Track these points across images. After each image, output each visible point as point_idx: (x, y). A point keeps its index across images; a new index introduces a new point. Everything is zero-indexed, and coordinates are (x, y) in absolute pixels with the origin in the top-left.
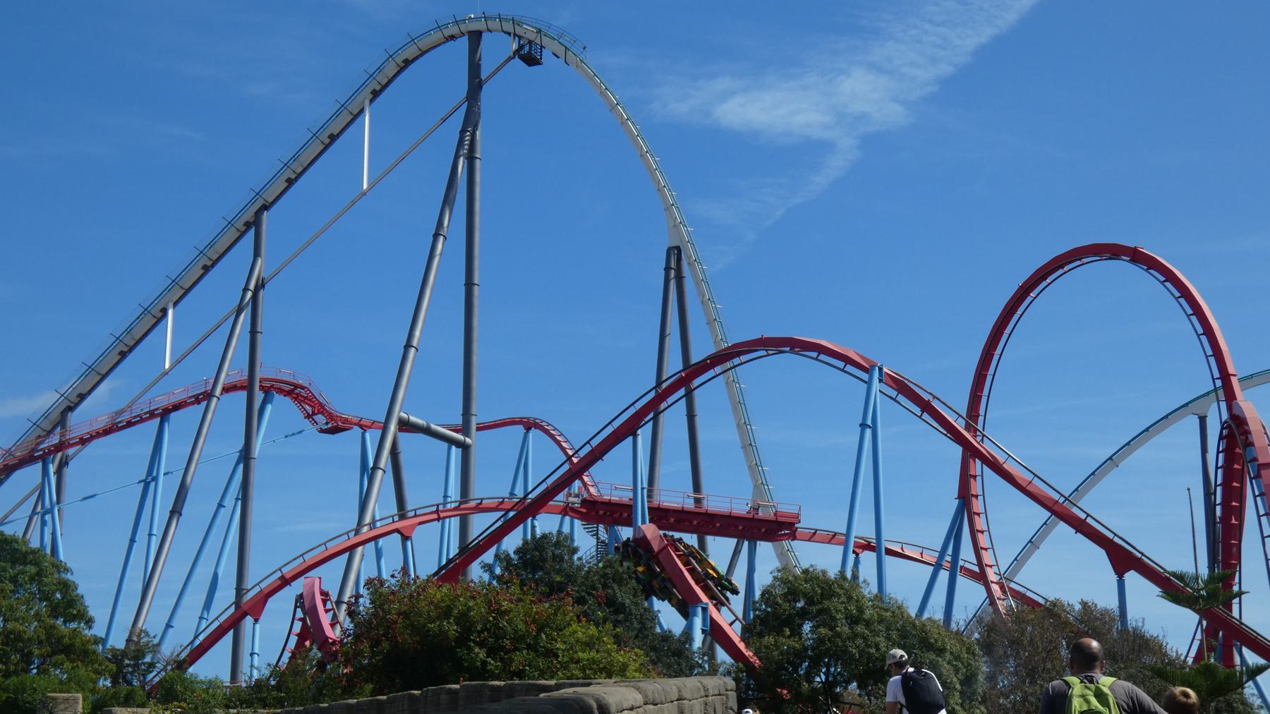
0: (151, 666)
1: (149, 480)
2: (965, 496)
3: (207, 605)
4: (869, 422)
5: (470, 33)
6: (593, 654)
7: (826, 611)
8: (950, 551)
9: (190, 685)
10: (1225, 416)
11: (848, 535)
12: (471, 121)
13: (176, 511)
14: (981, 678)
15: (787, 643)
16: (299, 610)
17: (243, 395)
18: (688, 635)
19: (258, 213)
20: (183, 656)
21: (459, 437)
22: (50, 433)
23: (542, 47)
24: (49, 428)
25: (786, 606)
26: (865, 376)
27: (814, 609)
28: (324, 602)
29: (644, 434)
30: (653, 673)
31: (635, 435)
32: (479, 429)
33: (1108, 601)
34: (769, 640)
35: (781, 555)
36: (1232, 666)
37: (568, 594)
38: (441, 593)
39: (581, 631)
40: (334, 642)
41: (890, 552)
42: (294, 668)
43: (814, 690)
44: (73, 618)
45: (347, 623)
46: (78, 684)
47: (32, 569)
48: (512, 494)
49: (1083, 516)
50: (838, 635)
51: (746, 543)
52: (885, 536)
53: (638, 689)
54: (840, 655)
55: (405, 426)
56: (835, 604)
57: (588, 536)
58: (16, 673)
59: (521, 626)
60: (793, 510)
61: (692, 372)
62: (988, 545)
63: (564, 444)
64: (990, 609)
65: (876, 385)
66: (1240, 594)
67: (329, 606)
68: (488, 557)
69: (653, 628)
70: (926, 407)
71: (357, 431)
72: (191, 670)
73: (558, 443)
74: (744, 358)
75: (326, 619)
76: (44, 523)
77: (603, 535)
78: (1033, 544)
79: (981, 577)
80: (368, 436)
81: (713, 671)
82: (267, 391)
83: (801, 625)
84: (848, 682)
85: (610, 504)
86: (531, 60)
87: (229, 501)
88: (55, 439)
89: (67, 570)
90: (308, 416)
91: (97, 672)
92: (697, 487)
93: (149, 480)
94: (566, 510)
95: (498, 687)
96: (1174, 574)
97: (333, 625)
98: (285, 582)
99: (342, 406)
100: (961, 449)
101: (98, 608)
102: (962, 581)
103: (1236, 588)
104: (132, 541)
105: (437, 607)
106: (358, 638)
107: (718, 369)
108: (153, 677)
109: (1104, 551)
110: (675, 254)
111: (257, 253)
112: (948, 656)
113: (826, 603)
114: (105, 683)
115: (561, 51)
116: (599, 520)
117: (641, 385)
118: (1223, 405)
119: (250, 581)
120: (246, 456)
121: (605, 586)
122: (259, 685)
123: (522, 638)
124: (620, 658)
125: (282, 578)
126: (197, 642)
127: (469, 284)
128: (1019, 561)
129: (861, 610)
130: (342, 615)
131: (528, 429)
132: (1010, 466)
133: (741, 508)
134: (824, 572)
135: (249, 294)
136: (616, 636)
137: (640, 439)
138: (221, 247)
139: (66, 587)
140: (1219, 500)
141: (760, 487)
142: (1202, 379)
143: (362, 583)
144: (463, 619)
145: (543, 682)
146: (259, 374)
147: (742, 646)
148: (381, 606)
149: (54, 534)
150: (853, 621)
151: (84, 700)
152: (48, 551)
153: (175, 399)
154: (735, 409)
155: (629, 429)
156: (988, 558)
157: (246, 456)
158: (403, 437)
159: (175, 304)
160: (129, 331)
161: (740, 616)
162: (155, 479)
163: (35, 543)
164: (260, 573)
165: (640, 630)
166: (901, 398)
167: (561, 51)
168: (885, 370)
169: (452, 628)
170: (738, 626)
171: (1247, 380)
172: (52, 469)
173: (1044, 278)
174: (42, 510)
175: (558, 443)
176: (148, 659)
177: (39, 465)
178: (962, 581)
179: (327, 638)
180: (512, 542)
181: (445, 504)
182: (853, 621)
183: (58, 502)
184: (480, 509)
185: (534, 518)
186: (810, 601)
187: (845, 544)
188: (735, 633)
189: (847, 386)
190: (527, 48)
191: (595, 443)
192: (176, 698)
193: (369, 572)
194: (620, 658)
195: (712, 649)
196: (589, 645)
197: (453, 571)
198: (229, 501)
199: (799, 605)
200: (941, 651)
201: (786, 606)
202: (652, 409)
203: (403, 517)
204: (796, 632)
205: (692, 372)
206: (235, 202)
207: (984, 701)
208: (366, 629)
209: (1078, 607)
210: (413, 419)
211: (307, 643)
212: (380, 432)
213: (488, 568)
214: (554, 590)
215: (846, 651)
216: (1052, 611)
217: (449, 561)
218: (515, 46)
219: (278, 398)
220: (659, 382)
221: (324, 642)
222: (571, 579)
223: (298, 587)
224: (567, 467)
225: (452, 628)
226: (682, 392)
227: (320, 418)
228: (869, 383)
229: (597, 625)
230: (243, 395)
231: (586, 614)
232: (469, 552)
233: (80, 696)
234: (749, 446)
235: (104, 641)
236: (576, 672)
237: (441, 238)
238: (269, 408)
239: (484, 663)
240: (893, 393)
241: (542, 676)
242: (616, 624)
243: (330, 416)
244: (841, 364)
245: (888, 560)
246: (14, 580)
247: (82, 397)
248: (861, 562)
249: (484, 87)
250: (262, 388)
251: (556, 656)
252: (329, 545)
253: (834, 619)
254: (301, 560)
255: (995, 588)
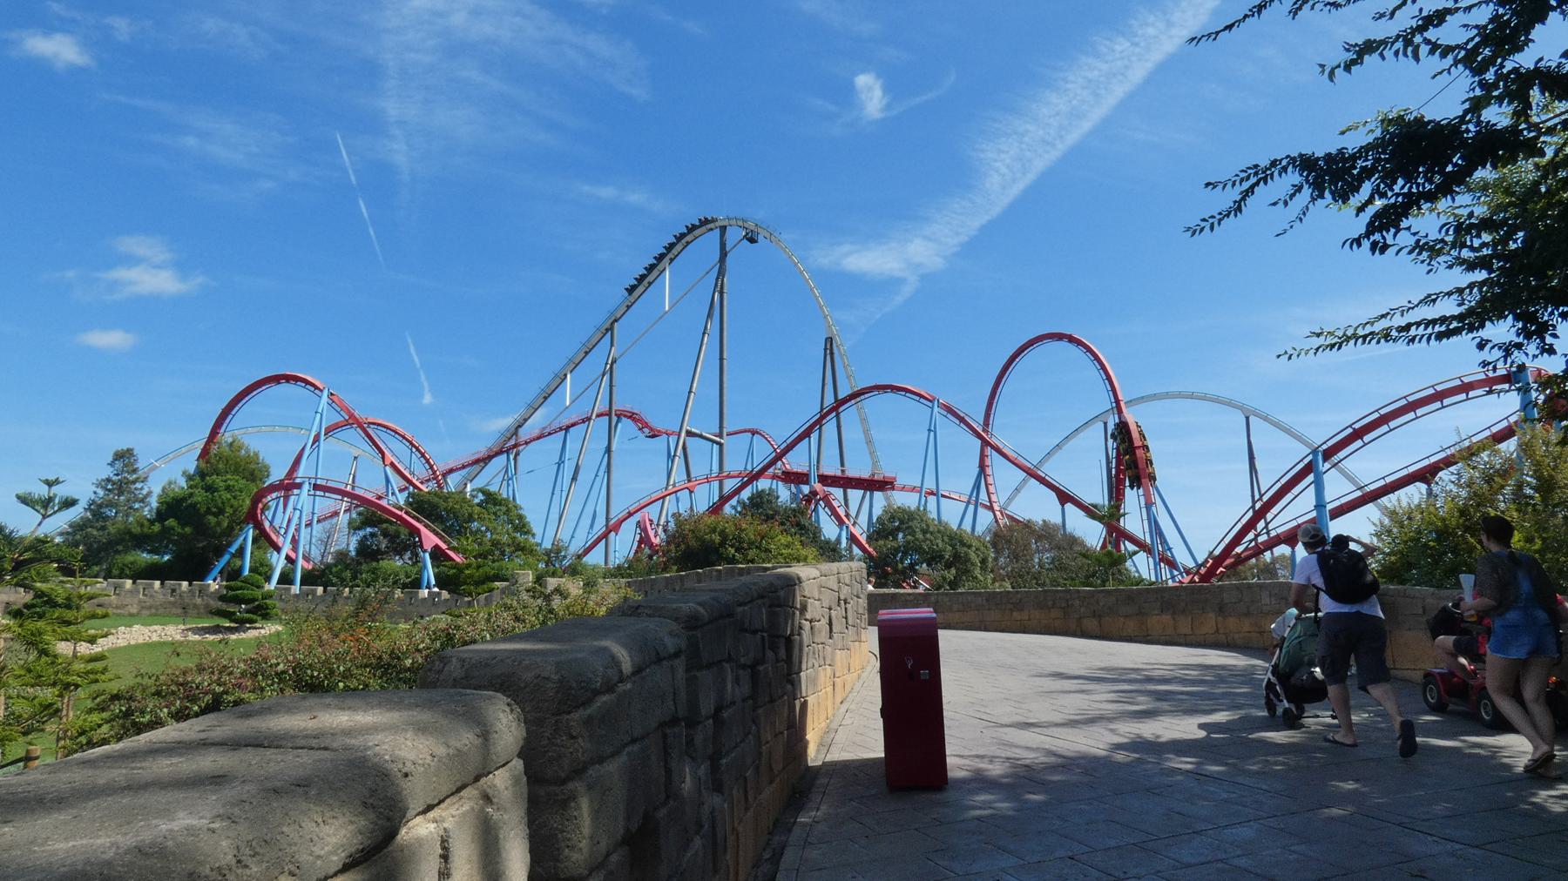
0: (565, 557)
1: (560, 463)
2: (982, 467)
3: (592, 526)
4: (932, 429)
5: (720, 227)
6: (790, 550)
7: (910, 527)
8: (975, 494)
9: (585, 566)
10: (1117, 421)
11: (921, 488)
12: (721, 273)
13: (574, 479)
14: (990, 560)
15: (890, 544)
16: (638, 529)
17: (607, 418)
18: (838, 540)
19: (612, 324)
20: (580, 552)
21: (718, 439)
22: (510, 439)
23: (758, 233)
24: (509, 436)
25: (890, 525)
26: (930, 404)
27: (904, 526)
28: (651, 525)
29: (814, 436)
30: (821, 560)
31: (810, 437)
32: (727, 435)
33: (1056, 519)
34: (881, 542)
35: (887, 499)
36: (1120, 551)
37: (776, 521)
38: (711, 520)
39: (784, 539)
40: (656, 545)
41: (943, 496)
42: (637, 559)
43: (904, 567)
44: (526, 533)
45: (663, 535)
46: (529, 565)
47: (504, 509)
48: (746, 469)
49: (1044, 476)
50: (917, 539)
51: (868, 493)
52: (941, 487)
53: (817, 569)
54: (918, 550)
55: (689, 434)
56: (915, 524)
57: (786, 490)
58: (498, 561)
59: (752, 537)
60: (894, 475)
61: (839, 403)
62: (994, 491)
63: (772, 443)
64: (995, 525)
65: (936, 409)
66: (1124, 515)
67: (653, 527)
68: (734, 501)
69: (820, 536)
70: (962, 420)
71: (665, 436)
72: (584, 559)
73: (766, 439)
74: (866, 396)
75: (652, 534)
76: (508, 485)
77: (794, 490)
78: (1017, 490)
79: (991, 508)
80: (670, 438)
81: (852, 559)
82: (618, 416)
83: (897, 535)
84: (922, 563)
85: (797, 473)
86: (752, 240)
87: (601, 473)
88: (512, 442)
89: (521, 508)
90: (640, 429)
91: (538, 560)
92: (842, 464)
93: (560, 463)
94: (774, 477)
95: (742, 569)
96: (1092, 505)
97: (655, 537)
98: (630, 514)
99: (658, 425)
100: (980, 442)
101: (537, 528)
102: (980, 510)
103: (1122, 511)
104: (553, 494)
105: (709, 527)
106: (668, 543)
107: (853, 402)
108: (566, 563)
109: (1054, 494)
110: (829, 340)
111: (612, 345)
112: (974, 549)
113: (910, 523)
114: (542, 566)
115: (768, 235)
116: (792, 482)
117: (813, 411)
118: (1116, 416)
119: (612, 515)
120: (608, 450)
121: (795, 516)
122: (619, 567)
123: (753, 543)
124: (804, 552)
125: (629, 512)
126: (587, 545)
127: (721, 359)
128: (1010, 499)
129: (928, 526)
130: (660, 530)
131: (753, 435)
132: (1005, 450)
133: (866, 475)
134: (909, 507)
135: (608, 366)
136: (801, 541)
137: (812, 439)
138: (594, 341)
139: (521, 517)
140: (1114, 466)
141: (875, 463)
142: (1106, 403)
143: (670, 515)
144: (723, 533)
145: (764, 565)
146: (614, 408)
147: (867, 546)
148: (680, 527)
149: (514, 490)
150: (924, 532)
151: (533, 574)
152: (511, 498)
153: (572, 421)
154: (862, 423)
155: (806, 434)
156: (994, 498)
157: (608, 450)
158: (689, 439)
159: (571, 372)
160: (548, 385)
161: (866, 530)
162: (563, 462)
163: (505, 496)
164: (617, 511)
165: (813, 538)
166: (949, 416)
167: (768, 235)
168: (941, 401)
169: (717, 538)
170: (865, 535)
171: (1128, 403)
172: (512, 457)
173: (1023, 351)
174: (508, 478)
175: (766, 439)
176: (563, 554)
177: (505, 455)
178: (980, 510)
179: (652, 543)
180: (746, 494)
181: (711, 474)
182: (924, 532)
183: (515, 474)
184: (729, 477)
185: (757, 480)
186: (902, 522)
187: (920, 492)
188: (863, 539)
189: (921, 410)
190: (750, 234)
191: (789, 442)
192: (578, 573)
193: (673, 510)
194: (804, 552)
195: (851, 547)
196: (787, 546)
197: (716, 509)
198: (601, 473)
199: (897, 524)
200: (970, 547)
201: (890, 525)
202: (819, 423)
203: (689, 481)
204: (895, 538)
205: (839, 403)
206: (600, 318)
207: (992, 571)
208: (672, 539)
209: (1041, 522)
210: (693, 430)
211: (643, 546)
212: (677, 437)
213: (734, 508)
214: (769, 518)
215: (921, 548)
216: (1028, 525)
217: (714, 504)
218: (744, 234)
219: (624, 419)
220: (822, 409)
221: (651, 545)
222: (777, 512)
223: (637, 517)
224: (774, 454)
225: (717, 538)
226: (834, 414)
227: (646, 430)
228: (932, 408)
229: (791, 536)
230: (607, 418)
231: (785, 530)
232: (724, 499)
233: (530, 572)
234: (869, 442)
235: (540, 545)
236: (782, 560)
237: (707, 335)
238: (620, 425)
239: (734, 556)
240: (945, 413)
241: (764, 562)
242: (801, 535)
243: (651, 429)
244: (918, 398)
245: (942, 500)
246: (495, 514)
247: (526, 420)
248: (1339, 533)
249: (728, 255)
250: (616, 415)
251: (771, 552)
252: (652, 496)
253: (915, 532)
254: (638, 504)
255: (998, 513)
